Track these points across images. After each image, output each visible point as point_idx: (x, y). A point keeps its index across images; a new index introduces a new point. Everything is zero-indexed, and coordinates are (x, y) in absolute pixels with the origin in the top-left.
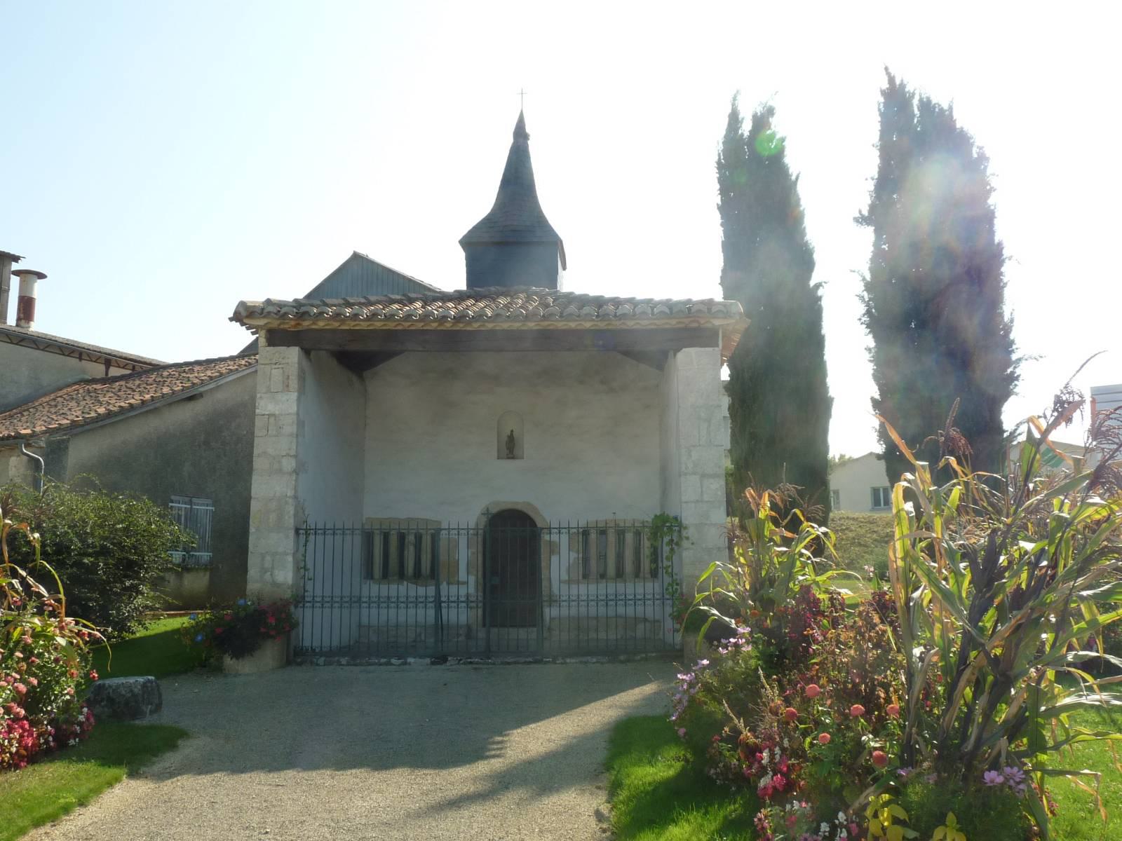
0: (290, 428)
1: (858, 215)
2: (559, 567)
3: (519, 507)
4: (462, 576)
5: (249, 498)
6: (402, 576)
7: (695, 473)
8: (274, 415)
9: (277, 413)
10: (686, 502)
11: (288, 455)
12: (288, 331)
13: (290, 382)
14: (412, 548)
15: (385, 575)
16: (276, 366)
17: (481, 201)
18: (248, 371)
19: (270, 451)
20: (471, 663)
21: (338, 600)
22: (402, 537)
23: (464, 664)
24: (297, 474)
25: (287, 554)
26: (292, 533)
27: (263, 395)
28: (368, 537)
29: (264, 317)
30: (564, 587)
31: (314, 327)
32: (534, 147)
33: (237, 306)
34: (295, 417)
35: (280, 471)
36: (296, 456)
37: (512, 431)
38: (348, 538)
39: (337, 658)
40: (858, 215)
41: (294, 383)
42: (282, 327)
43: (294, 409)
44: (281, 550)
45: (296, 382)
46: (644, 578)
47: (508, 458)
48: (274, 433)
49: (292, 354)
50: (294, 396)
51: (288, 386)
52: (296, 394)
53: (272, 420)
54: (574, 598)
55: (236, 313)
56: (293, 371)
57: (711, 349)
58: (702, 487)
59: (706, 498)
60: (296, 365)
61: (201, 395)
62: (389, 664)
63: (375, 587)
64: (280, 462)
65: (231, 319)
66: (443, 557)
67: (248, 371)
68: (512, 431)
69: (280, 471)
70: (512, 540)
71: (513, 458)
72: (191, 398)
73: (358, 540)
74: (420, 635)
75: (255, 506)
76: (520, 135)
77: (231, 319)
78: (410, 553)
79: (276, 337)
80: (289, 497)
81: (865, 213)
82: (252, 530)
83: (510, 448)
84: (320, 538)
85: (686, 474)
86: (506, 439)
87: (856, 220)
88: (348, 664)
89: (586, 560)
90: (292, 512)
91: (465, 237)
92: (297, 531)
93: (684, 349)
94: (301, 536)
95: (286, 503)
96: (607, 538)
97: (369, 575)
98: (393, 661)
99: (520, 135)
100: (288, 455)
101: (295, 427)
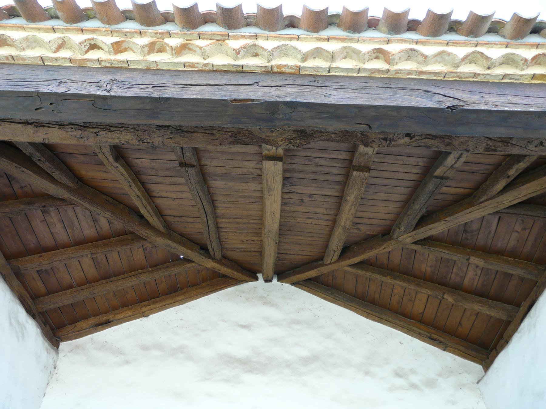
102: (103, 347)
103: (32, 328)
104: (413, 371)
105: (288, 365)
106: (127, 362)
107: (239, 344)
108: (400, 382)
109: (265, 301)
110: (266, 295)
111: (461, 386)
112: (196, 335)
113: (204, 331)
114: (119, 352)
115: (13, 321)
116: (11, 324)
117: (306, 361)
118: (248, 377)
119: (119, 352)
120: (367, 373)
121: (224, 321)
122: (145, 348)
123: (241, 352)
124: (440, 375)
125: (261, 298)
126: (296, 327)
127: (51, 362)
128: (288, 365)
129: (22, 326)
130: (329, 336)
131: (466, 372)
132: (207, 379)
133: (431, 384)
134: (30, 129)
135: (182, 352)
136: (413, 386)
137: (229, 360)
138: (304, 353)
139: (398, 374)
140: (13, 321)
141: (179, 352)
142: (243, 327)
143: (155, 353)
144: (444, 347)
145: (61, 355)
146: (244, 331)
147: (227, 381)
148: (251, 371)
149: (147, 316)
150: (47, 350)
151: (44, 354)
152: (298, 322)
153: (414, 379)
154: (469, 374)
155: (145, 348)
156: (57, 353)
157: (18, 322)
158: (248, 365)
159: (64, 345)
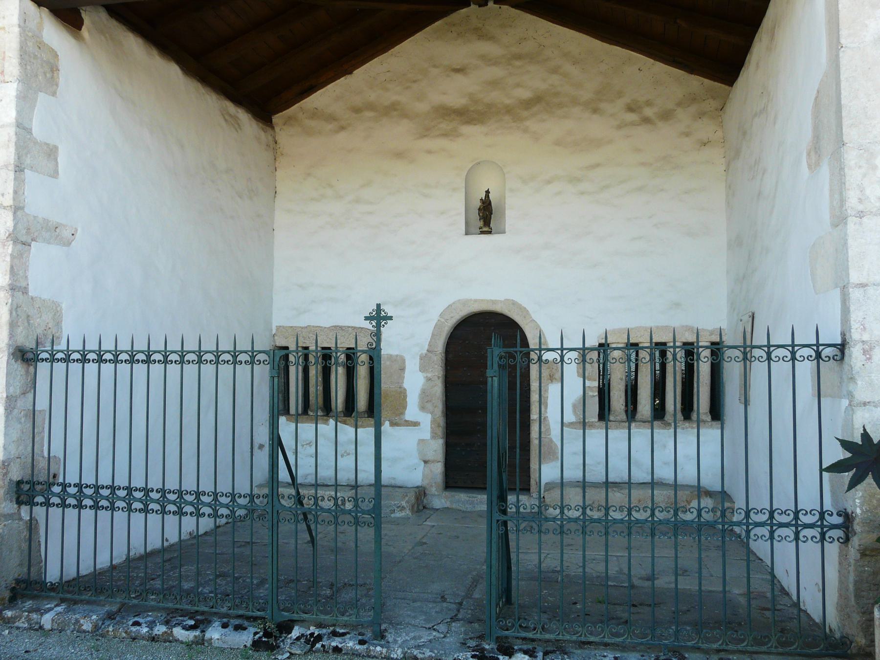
2: (560, 398)
3: (498, 308)
4: (412, 412)
10: (863, 286)
14: (341, 370)
18: (493, 612)
21: (152, 506)
30: (573, 436)
37: (488, 192)
38: (781, 369)
46: (698, 422)
47: (482, 233)
54: (784, 519)
66: (386, 384)
67: (493, 612)
68: (488, 192)
70: (486, 356)
71: (490, 233)
78: (339, 377)
83: (485, 216)
85: (861, 215)
86: (478, 204)
89: (604, 393)
94: (756, 365)
96: (11, 335)
102: (315, 114)
103: (243, 116)
104: (649, 103)
105: (508, 110)
106: (342, 128)
107: (453, 91)
108: (632, 117)
109: (482, 35)
110: (480, 25)
111: (701, 115)
112: (407, 88)
113: (415, 82)
114: (331, 118)
115: (227, 117)
116: (226, 120)
117: (528, 104)
118: (466, 129)
119: (331, 118)
120: (595, 111)
121: (435, 66)
122: (357, 110)
123: (455, 100)
124: (679, 104)
125: (476, 29)
126: (517, 63)
127: (270, 138)
128: (508, 110)
129: (235, 118)
130: (555, 71)
131: (712, 97)
132: (425, 136)
133: (666, 116)
134: (538, 436)
135: (395, 110)
136: (646, 120)
137: (446, 112)
138: (525, 94)
139: (630, 109)
140: (227, 117)
141: (392, 111)
142: (457, 71)
143: (369, 114)
144: (691, 70)
145: (277, 129)
146: (459, 77)
147: (445, 135)
148: (470, 121)
149: (351, 73)
150: (263, 129)
151: (262, 133)
152: (518, 57)
153: (649, 112)
154: (714, 99)
155: (357, 110)
156: (273, 128)
157: (230, 115)
158: (468, 115)
159: (277, 119)
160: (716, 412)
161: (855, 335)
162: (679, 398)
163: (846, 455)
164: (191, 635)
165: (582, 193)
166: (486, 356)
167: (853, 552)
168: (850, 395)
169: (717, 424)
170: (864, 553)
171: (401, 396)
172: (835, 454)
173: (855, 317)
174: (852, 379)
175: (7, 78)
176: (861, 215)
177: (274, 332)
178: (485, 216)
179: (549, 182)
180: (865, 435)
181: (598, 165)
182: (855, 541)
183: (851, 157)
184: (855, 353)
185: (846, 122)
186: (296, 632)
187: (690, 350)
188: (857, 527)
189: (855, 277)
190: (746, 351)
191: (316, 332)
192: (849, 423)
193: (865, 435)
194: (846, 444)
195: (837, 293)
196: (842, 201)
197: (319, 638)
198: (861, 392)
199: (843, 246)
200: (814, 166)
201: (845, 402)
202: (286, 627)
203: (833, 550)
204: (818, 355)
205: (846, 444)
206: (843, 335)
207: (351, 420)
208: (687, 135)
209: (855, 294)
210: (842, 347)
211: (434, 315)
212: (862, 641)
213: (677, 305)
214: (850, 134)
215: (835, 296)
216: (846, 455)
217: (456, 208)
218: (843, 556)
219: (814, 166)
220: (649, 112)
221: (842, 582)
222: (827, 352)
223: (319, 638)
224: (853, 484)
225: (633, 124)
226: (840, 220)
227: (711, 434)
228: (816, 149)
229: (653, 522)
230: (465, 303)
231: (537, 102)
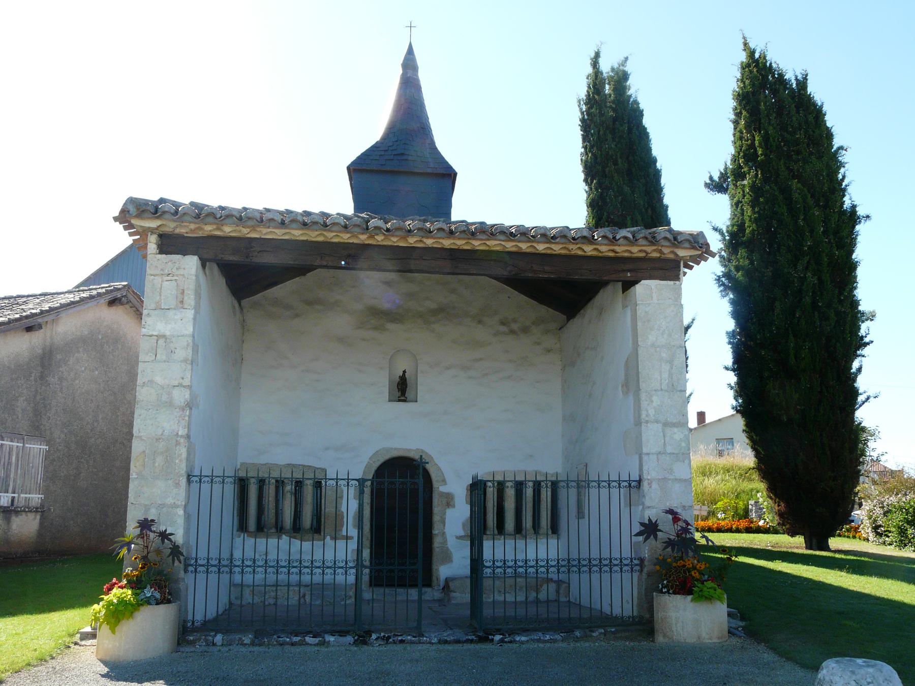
0: (183, 352)
1: (708, 181)
2: (453, 522)
3: (411, 455)
5: (130, 435)
6: (279, 530)
7: (657, 422)
8: (164, 336)
9: (168, 333)
10: (648, 454)
11: (180, 385)
12: (184, 237)
13: (186, 298)
15: (260, 528)
16: (169, 278)
17: (370, 128)
19: (159, 379)
20: (402, 641)
22: (537, 485)
23: (394, 642)
24: (191, 409)
25: (177, 507)
26: (183, 481)
27: (151, 312)
28: (242, 484)
29: (158, 218)
31: (218, 233)
32: (424, 77)
33: (125, 204)
34: (190, 340)
35: (170, 404)
36: (190, 387)
39: (237, 637)
40: (708, 181)
41: (190, 299)
42: (178, 231)
43: (190, 329)
44: (170, 501)
45: (192, 297)
47: (399, 401)
48: (164, 357)
49: (191, 263)
50: (190, 314)
51: (182, 302)
52: (193, 311)
53: (161, 342)
55: (124, 212)
56: (190, 285)
57: (672, 282)
58: (664, 436)
59: (669, 449)
60: (194, 278)
61: (40, 327)
62: (303, 643)
63: (250, 541)
64: (170, 394)
65: (116, 219)
66: (328, 508)
68: (404, 372)
69: (170, 404)
70: (401, 491)
71: (405, 401)
72: (29, 329)
73: (230, 490)
74: (304, 596)
75: (137, 447)
76: (410, 64)
77: (116, 219)
79: (170, 244)
80: (181, 436)
81: (716, 178)
82: (133, 475)
83: (402, 389)
84: (604, 492)
85: (647, 422)
87: (707, 185)
88: (253, 644)
90: (184, 455)
91: (353, 163)
92: (189, 477)
93: (643, 282)
95: (178, 443)
97: (242, 527)
98: (309, 639)
99: (410, 64)
100: (180, 385)
101: (190, 351)
106: (297, 316)
108: (503, 328)
111: (547, 332)
114: (288, 307)
118: (391, 326)
120: (480, 322)
124: (533, 323)
133: (525, 330)
136: (513, 332)
138: (433, 305)
139: (503, 323)
147: (376, 328)
153: (515, 326)
155: (309, 303)
160: (555, 529)
161: (645, 476)
162: (549, 513)
163: (643, 528)
164: (317, 640)
165: (470, 378)
166: (401, 491)
167: (644, 575)
168: (643, 504)
169: (555, 536)
170: (649, 575)
171: (338, 518)
172: (637, 528)
173: (645, 468)
174: (644, 496)
175: (186, 306)
176: (647, 422)
177: (239, 467)
178: (402, 389)
179: (448, 368)
180: (650, 520)
181: (481, 359)
182: (645, 570)
183: (643, 396)
184: (645, 484)
185: (641, 380)
186: (374, 636)
187: (537, 485)
188: (646, 563)
189: (645, 450)
190: (582, 485)
191: (270, 467)
192: (643, 516)
193: (650, 520)
194: (642, 524)
195: (637, 457)
196: (640, 415)
197: (389, 637)
198: (648, 503)
199: (639, 435)
200: (626, 393)
201: (641, 507)
202: (369, 633)
203: (636, 575)
204: (630, 485)
205: (642, 524)
206: (640, 476)
207: (298, 535)
208: (538, 344)
209: (645, 458)
210: (639, 482)
211: (365, 459)
212: (647, 616)
213: (531, 456)
214: (643, 385)
215: (637, 457)
216: (643, 528)
217: (383, 383)
218: (639, 579)
219: (626, 393)
220: (515, 326)
221: (639, 593)
222: (633, 484)
223: (389, 637)
224: (645, 540)
225: (504, 333)
226: (638, 423)
227: (553, 542)
228: (626, 385)
229: (516, 602)
230: (388, 450)
231: (442, 313)
